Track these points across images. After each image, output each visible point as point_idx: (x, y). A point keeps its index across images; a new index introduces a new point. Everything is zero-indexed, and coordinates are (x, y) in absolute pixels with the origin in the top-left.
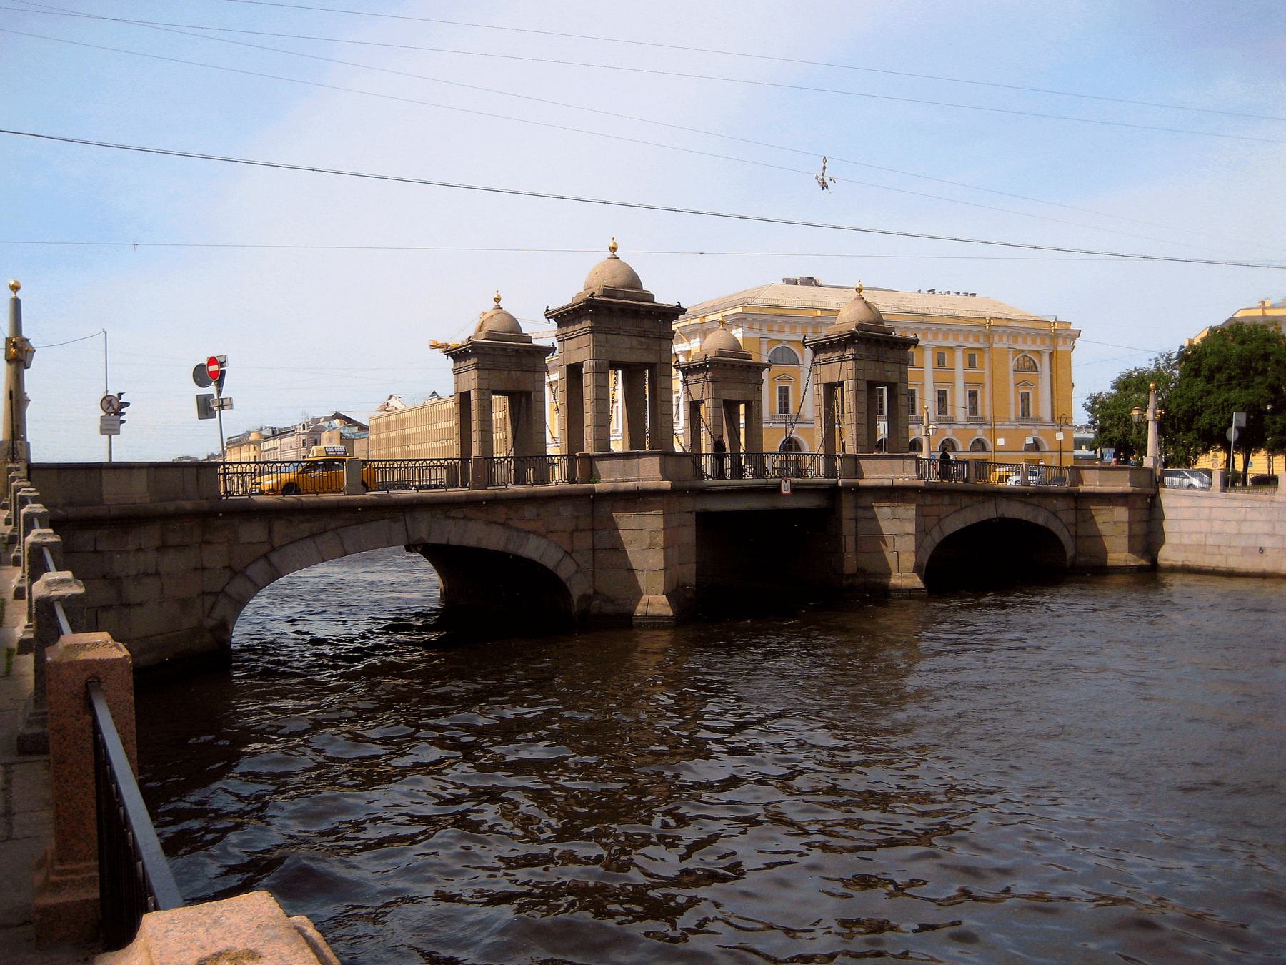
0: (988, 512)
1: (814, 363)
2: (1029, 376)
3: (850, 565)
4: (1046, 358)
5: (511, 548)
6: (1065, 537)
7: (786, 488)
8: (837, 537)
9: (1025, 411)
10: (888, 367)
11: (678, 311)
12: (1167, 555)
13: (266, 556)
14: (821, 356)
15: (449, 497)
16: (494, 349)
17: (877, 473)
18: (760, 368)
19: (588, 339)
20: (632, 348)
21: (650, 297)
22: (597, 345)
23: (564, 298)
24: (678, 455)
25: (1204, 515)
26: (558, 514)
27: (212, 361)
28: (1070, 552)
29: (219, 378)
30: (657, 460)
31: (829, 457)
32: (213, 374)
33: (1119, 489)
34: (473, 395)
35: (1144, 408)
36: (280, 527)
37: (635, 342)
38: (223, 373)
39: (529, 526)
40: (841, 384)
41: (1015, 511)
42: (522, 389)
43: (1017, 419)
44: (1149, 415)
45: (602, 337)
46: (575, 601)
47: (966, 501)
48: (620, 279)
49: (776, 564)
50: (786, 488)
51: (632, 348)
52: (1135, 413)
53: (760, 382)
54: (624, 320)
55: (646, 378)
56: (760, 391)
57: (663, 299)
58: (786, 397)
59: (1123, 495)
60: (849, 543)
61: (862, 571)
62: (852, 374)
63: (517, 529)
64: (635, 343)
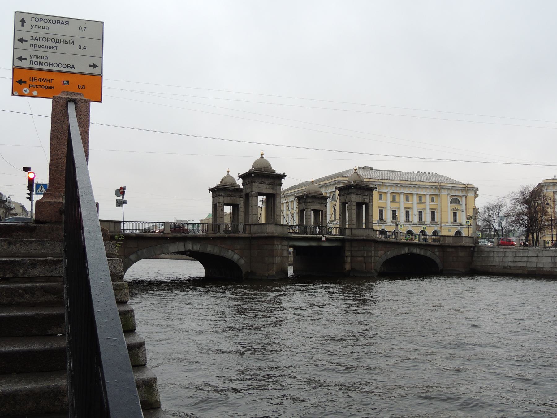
0: (406, 250)
2: (457, 206)
6: (438, 261)
7: (324, 239)
9: (455, 220)
10: (365, 197)
11: (283, 176)
20: (266, 188)
21: (274, 171)
23: (245, 170)
24: (282, 225)
27: (121, 188)
29: (123, 194)
37: (267, 186)
42: (235, 203)
43: (452, 223)
46: (244, 273)
50: (324, 239)
51: (266, 188)
53: (326, 203)
54: (263, 177)
55: (272, 199)
56: (326, 206)
57: (278, 172)
58: (382, 214)
64: (268, 187)
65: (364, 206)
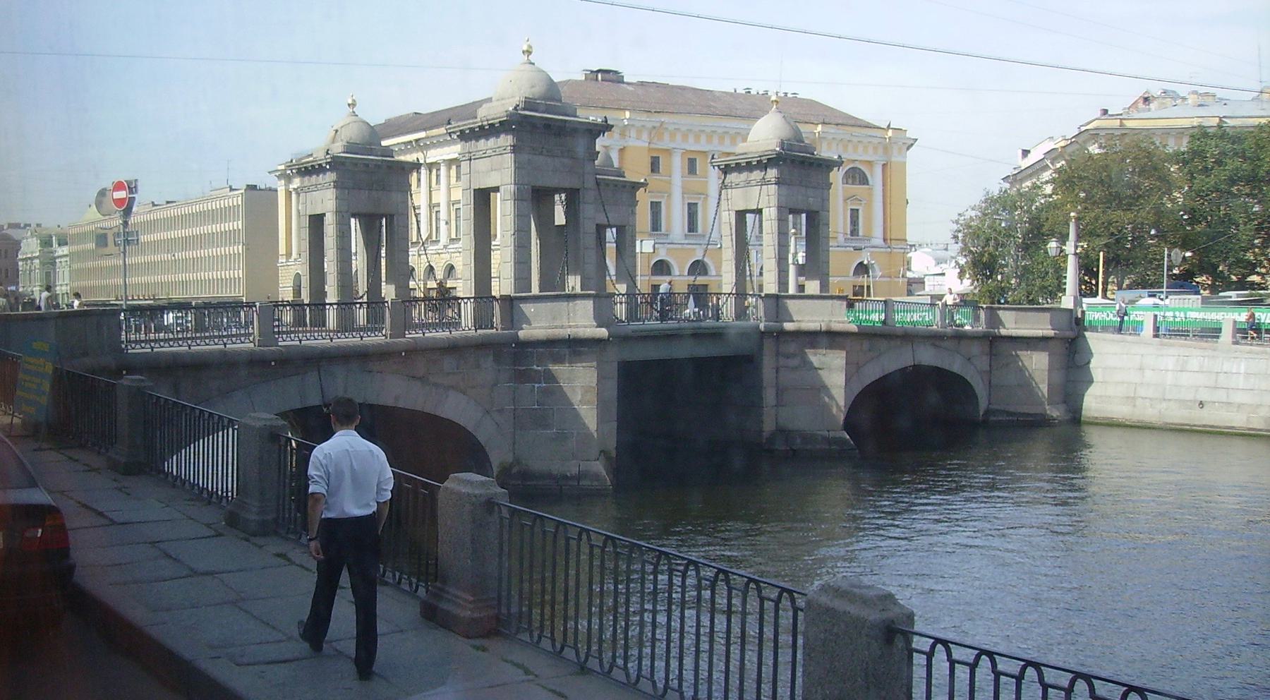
1: (724, 186)
2: (858, 189)
3: (768, 426)
4: (878, 170)
8: (756, 388)
12: (1094, 402)
14: (733, 177)
15: (338, 348)
16: (367, 166)
17: (808, 316)
18: (635, 186)
19: (509, 159)
22: (519, 167)
25: (1155, 363)
27: (119, 186)
28: (983, 405)
30: (590, 304)
31: (740, 295)
32: (119, 202)
33: (1039, 333)
34: (330, 220)
35: (1063, 239)
38: (132, 200)
40: (759, 212)
41: (927, 356)
44: (1069, 248)
45: (525, 157)
47: (883, 344)
48: (538, 90)
49: (705, 425)
52: (1053, 245)
59: (1044, 339)
60: (769, 396)
61: (781, 431)
62: (774, 201)
63: (436, 385)
65: (804, 216)
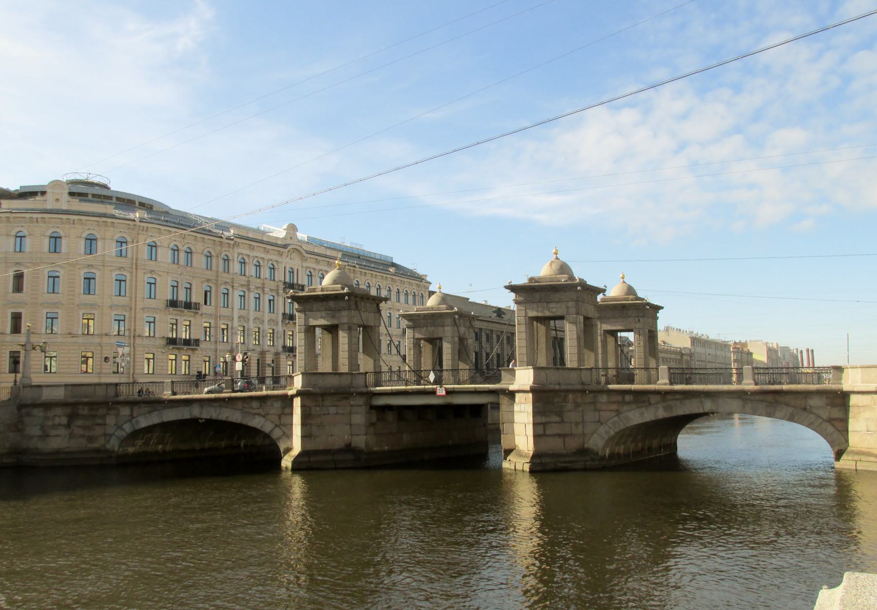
5: (244, 422)
13: (130, 421)
26: (272, 405)
36: (136, 411)
39: (256, 411)
42: (435, 336)
63: (248, 413)
